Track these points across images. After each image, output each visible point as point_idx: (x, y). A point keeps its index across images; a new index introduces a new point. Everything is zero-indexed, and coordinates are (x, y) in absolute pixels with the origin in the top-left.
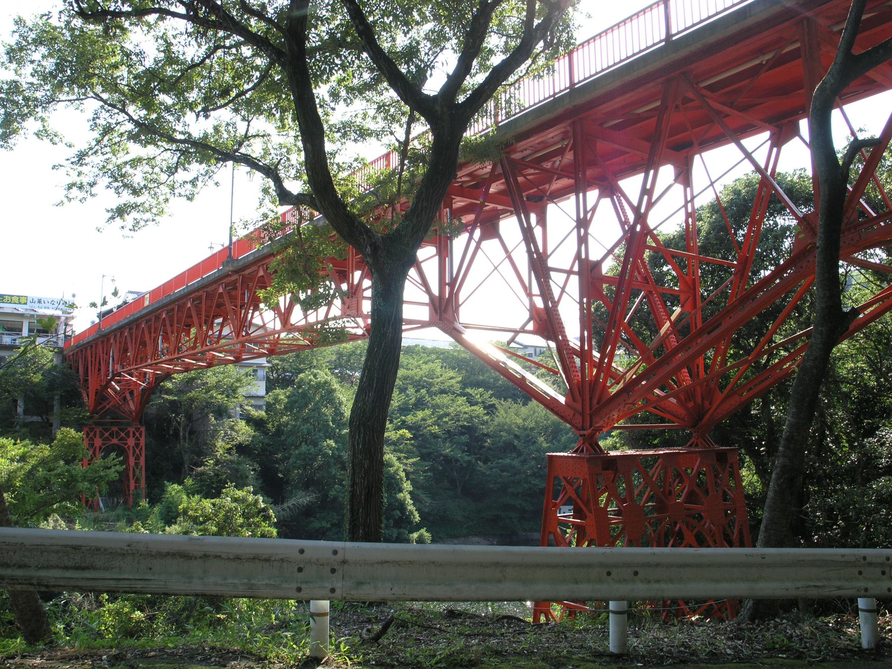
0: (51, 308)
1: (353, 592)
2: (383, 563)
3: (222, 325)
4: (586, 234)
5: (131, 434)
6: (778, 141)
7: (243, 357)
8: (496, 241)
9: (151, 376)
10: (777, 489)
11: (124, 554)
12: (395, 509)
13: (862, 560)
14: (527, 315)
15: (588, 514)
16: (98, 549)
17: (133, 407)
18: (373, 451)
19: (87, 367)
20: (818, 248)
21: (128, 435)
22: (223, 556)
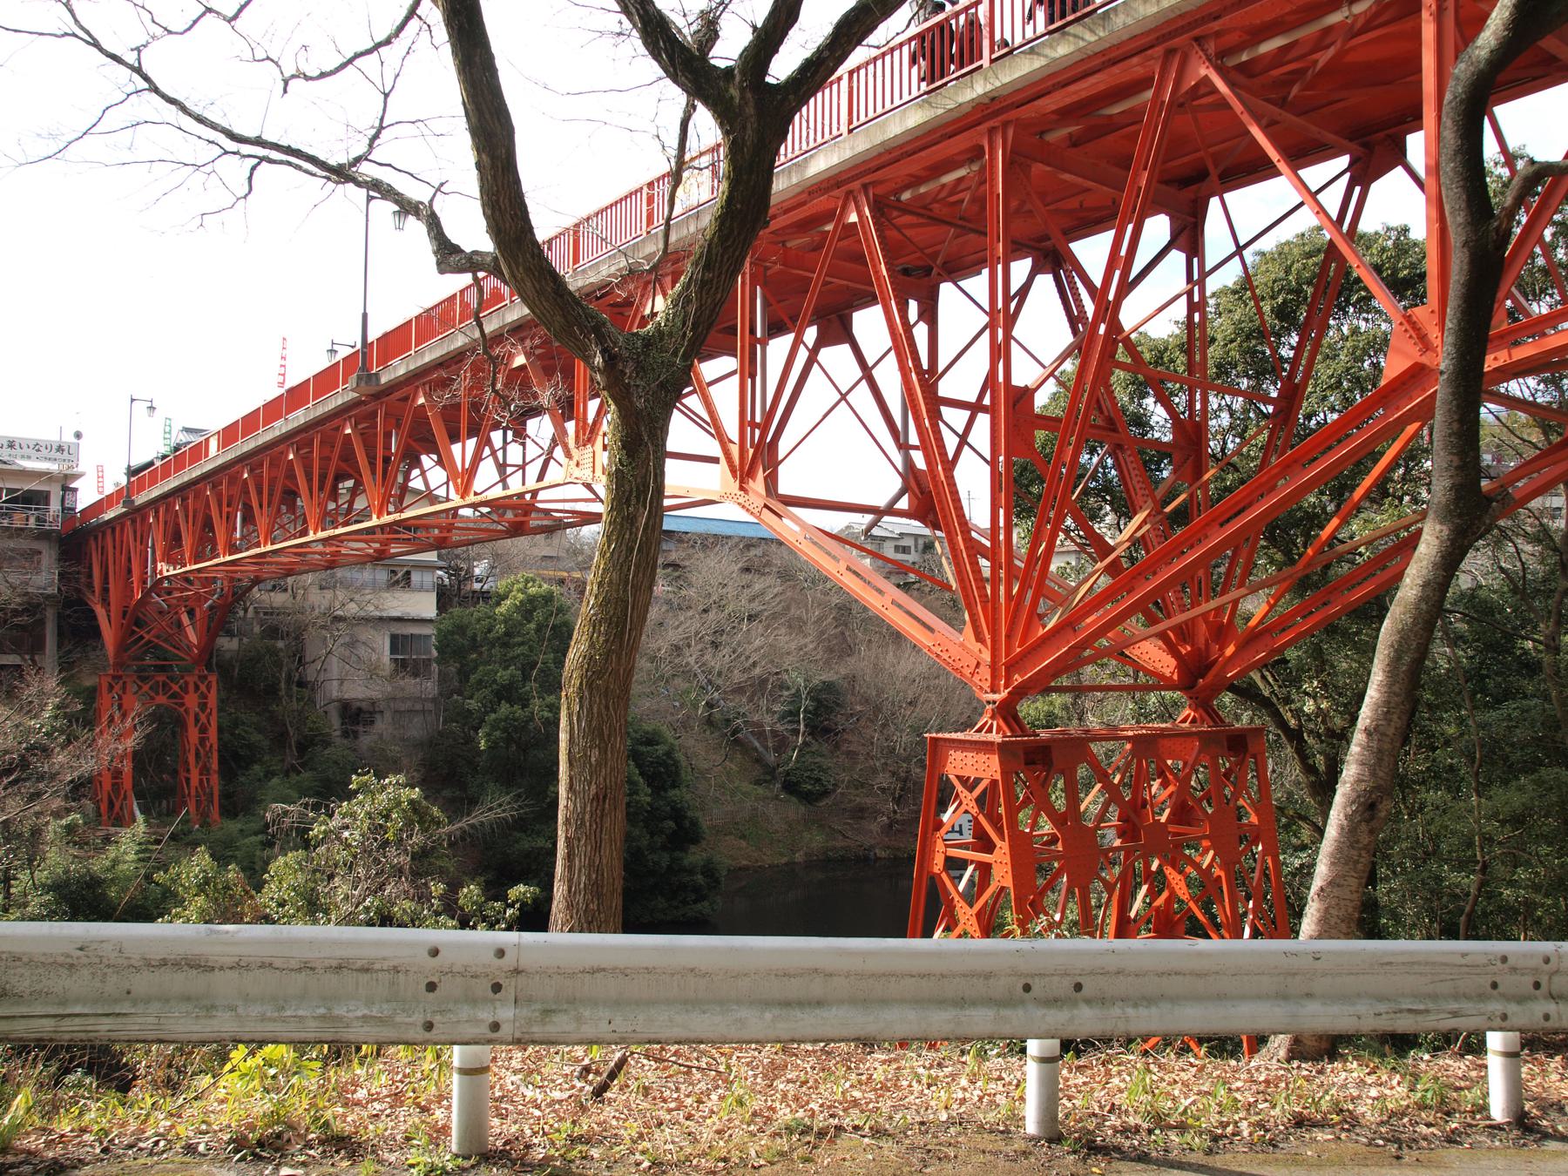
0: (34, 457)
1: (535, 1029)
2: (594, 971)
3: (354, 492)
4: (1008, 336)
5: (191, 687)
6: (1363, 175)
7: (392, 551)
8: (845, 349)
9: (226, 583)
10: (1345, 823)
11: (72, 965)
12: (665, 819)
13: (1499, 963)
14: (897, 483)
15: (999, 843)
16: (16, 958)
17: (193, 639)
18: (606, 732)
19: (107, 567)
20: (1442, 373)
21: (185, 689)
22: (278, 963)
